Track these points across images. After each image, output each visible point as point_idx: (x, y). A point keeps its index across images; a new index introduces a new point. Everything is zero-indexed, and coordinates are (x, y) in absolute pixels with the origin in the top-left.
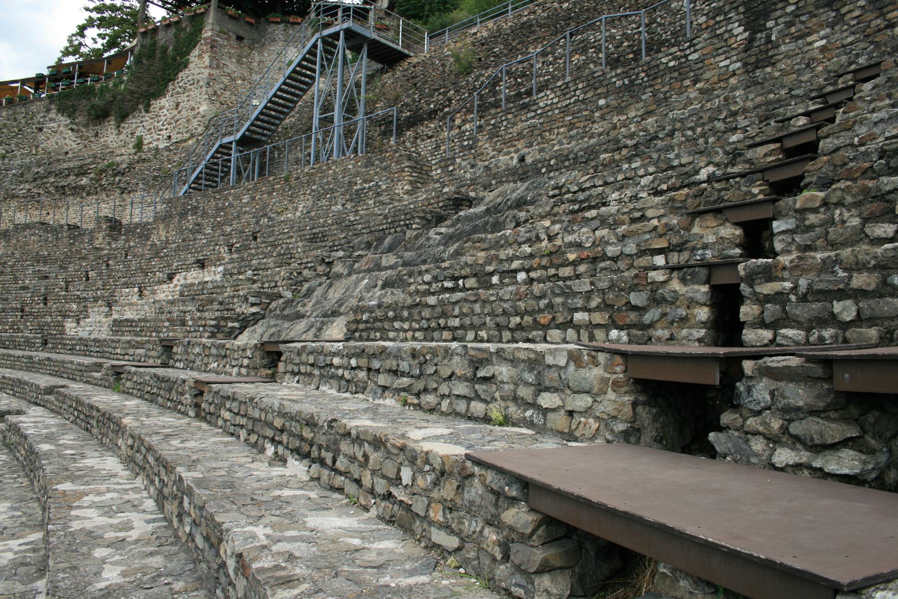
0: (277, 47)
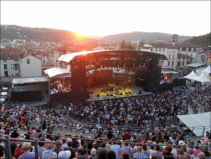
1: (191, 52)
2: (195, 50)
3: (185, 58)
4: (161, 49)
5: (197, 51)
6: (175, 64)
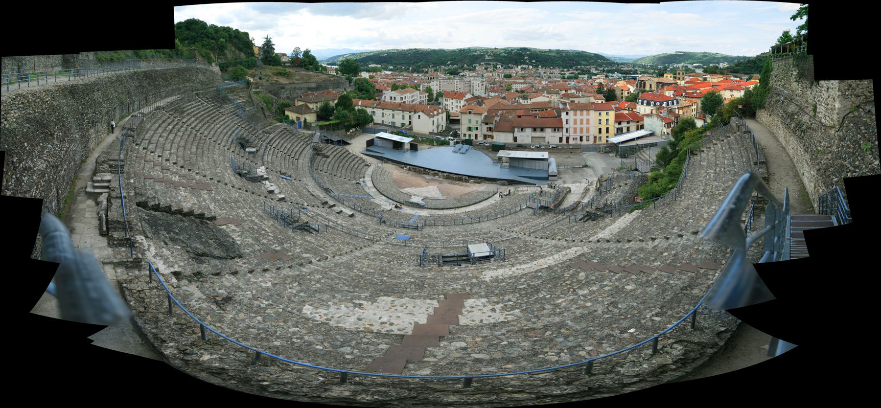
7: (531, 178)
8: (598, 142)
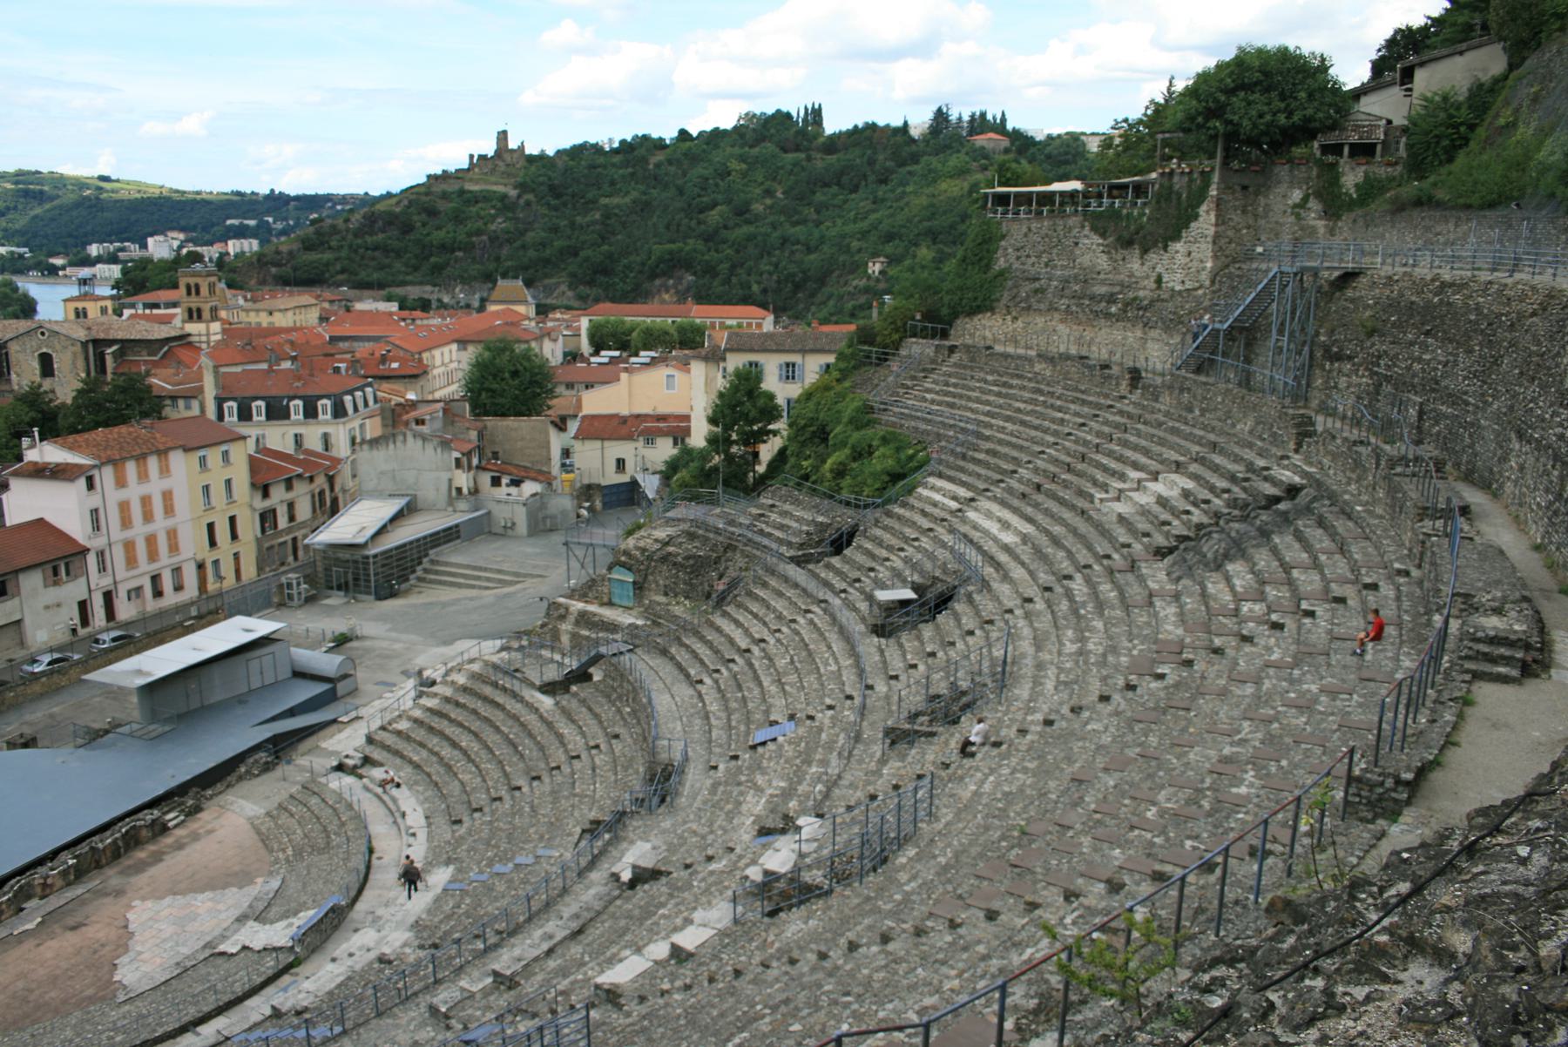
0: (1281, 189)
1: (319, 423)
2: (339, 412)
3: (296, 483)
4: (145, 465)
5: (350, 410)
6: (249, 528)
7: (291, 713)
8: (212, 586)
